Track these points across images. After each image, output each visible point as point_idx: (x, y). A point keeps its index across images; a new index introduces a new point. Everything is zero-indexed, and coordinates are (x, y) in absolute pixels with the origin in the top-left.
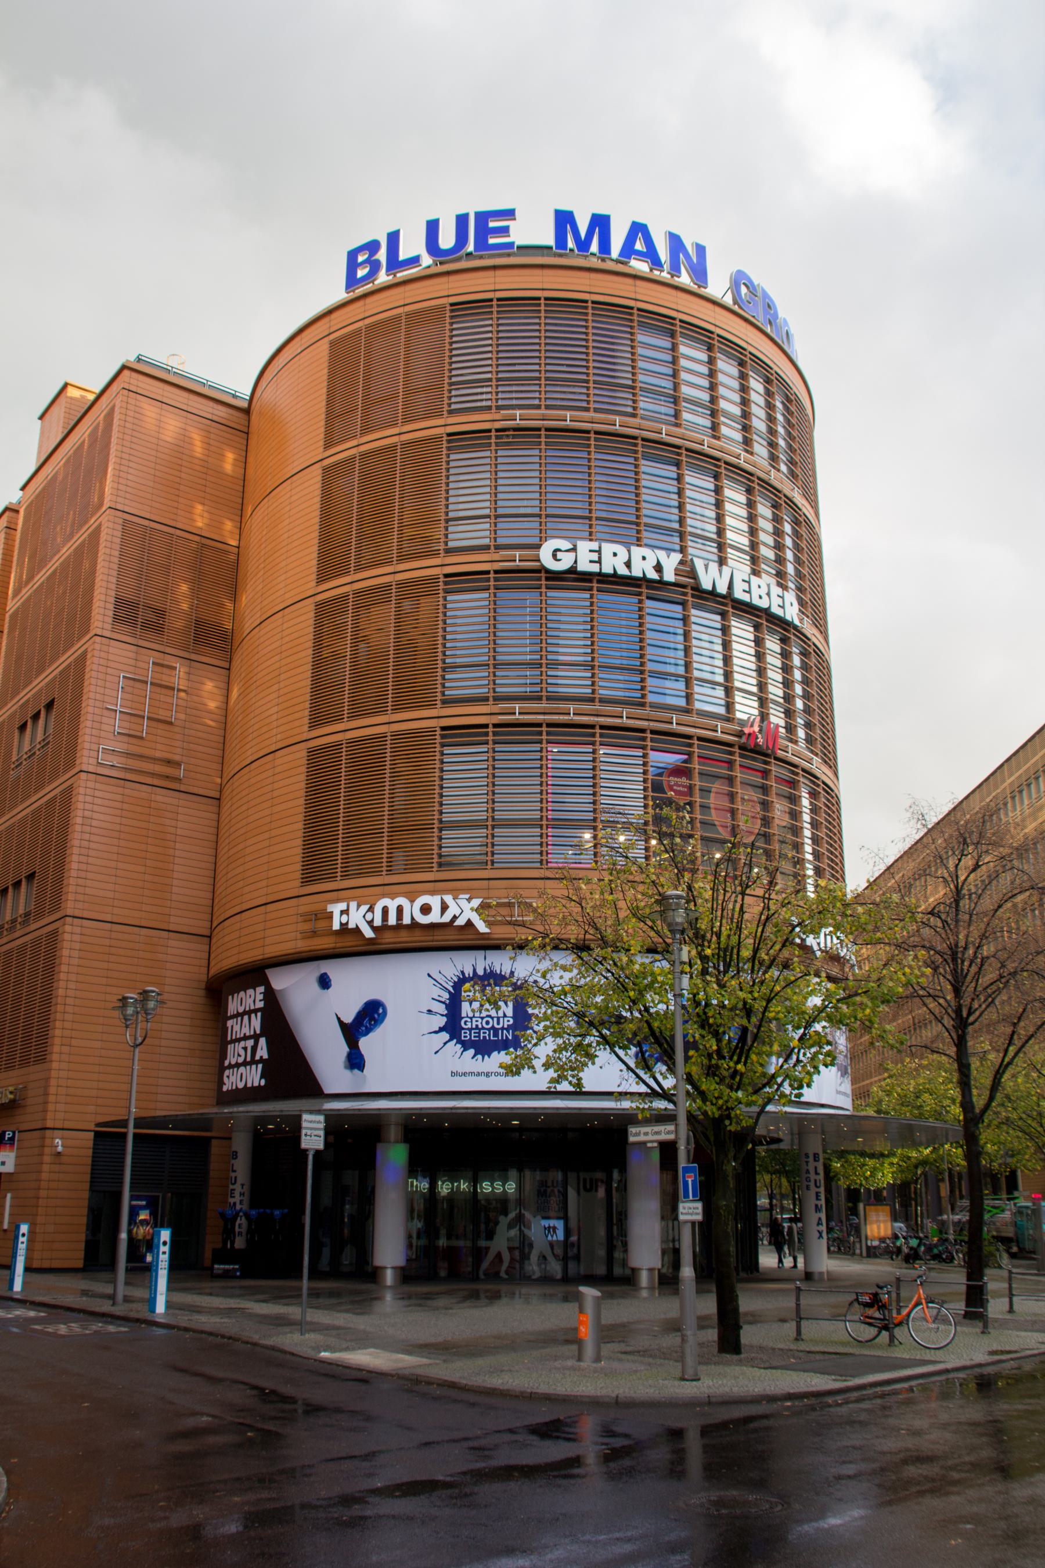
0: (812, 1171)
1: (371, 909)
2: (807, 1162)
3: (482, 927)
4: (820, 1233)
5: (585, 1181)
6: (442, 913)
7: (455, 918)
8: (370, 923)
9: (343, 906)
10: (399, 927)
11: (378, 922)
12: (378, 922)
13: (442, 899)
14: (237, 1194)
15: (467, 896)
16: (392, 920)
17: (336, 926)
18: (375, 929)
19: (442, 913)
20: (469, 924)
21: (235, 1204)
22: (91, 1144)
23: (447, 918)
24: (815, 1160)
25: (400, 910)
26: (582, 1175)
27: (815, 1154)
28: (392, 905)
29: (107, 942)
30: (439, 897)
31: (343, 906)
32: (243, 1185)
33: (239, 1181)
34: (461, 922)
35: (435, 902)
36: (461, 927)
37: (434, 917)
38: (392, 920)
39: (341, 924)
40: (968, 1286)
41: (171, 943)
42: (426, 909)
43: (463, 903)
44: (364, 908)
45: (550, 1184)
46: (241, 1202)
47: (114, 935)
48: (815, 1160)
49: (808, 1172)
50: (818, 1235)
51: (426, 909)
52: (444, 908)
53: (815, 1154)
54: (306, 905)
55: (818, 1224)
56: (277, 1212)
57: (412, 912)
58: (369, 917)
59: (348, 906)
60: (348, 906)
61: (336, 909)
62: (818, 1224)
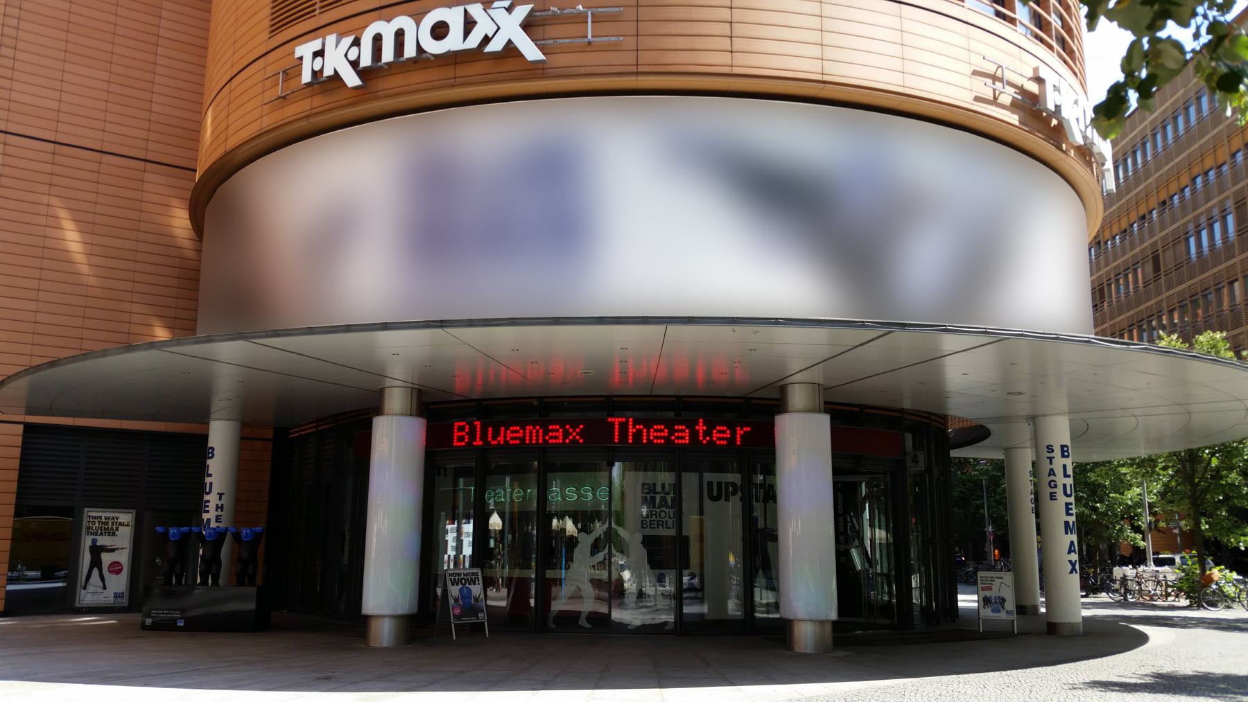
0: (1059, 472)
1: (356, 43)
2: (1051, 459)
3: (530, 51)
4: (1073, 564)
5: (710, 484)
6: (467, 33)
7: (486, 40)
8: (355, 64)
9: (316, 45)
10: (400, 64)
11: (366, 61)
12: (366, 61)
13: (466, 11)
14: (212, 507)
15: (507, 4)
16: (388, 55)
17: (306, 77)
18: (362, 73)
19: (467, 33)
20: (510, 50)
21: (209, 520)
22: (19, 440)
23: (474, 41)
24: (1063, 456)
25: (400, 34)
26: (708, 477)
27: (1062, 447)
28: (388, 30)
29: (48, 168)
30: (460, 10)
31: (316, 45)
32: (220, 495)
33: (216, 490)
34: (496, 46)
35: (454, 17)
36: (495, 56)
37: (454, 42)
38: (388, 55)
39: (315, 73)
40: (29, 429)
41: (148, 176)
42: (440, 31)
43: (499, 14)
44: (348, 40)
45: (659, 489)
46: (218, 519)
47: (59, 159)
48: (1063, 456)
49: (1052, 473)
50: (1070, 567)
51: (440, 31)
52: (469, 24)
53: (1062, 447)
54: (274, 64)
55: (1069, 552)
56: (172, 531)
57: (418, 36)
58: (353, 55)
59: (324, 45)
60: (324, 45)
61: (305, 50)
62: (1069, 552)
